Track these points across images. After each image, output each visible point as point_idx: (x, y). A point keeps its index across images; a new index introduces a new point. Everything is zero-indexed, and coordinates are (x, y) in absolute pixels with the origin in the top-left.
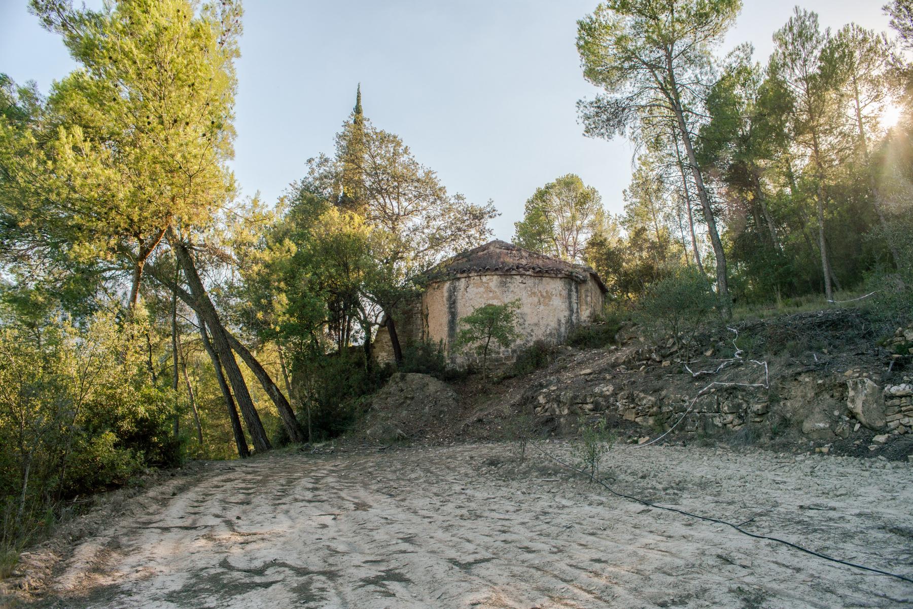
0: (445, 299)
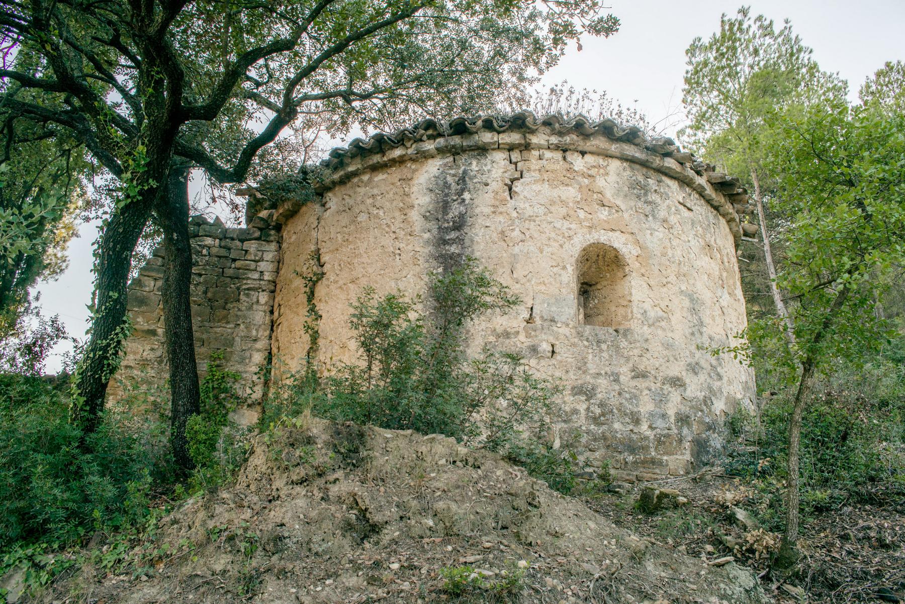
0: (415, 216)
